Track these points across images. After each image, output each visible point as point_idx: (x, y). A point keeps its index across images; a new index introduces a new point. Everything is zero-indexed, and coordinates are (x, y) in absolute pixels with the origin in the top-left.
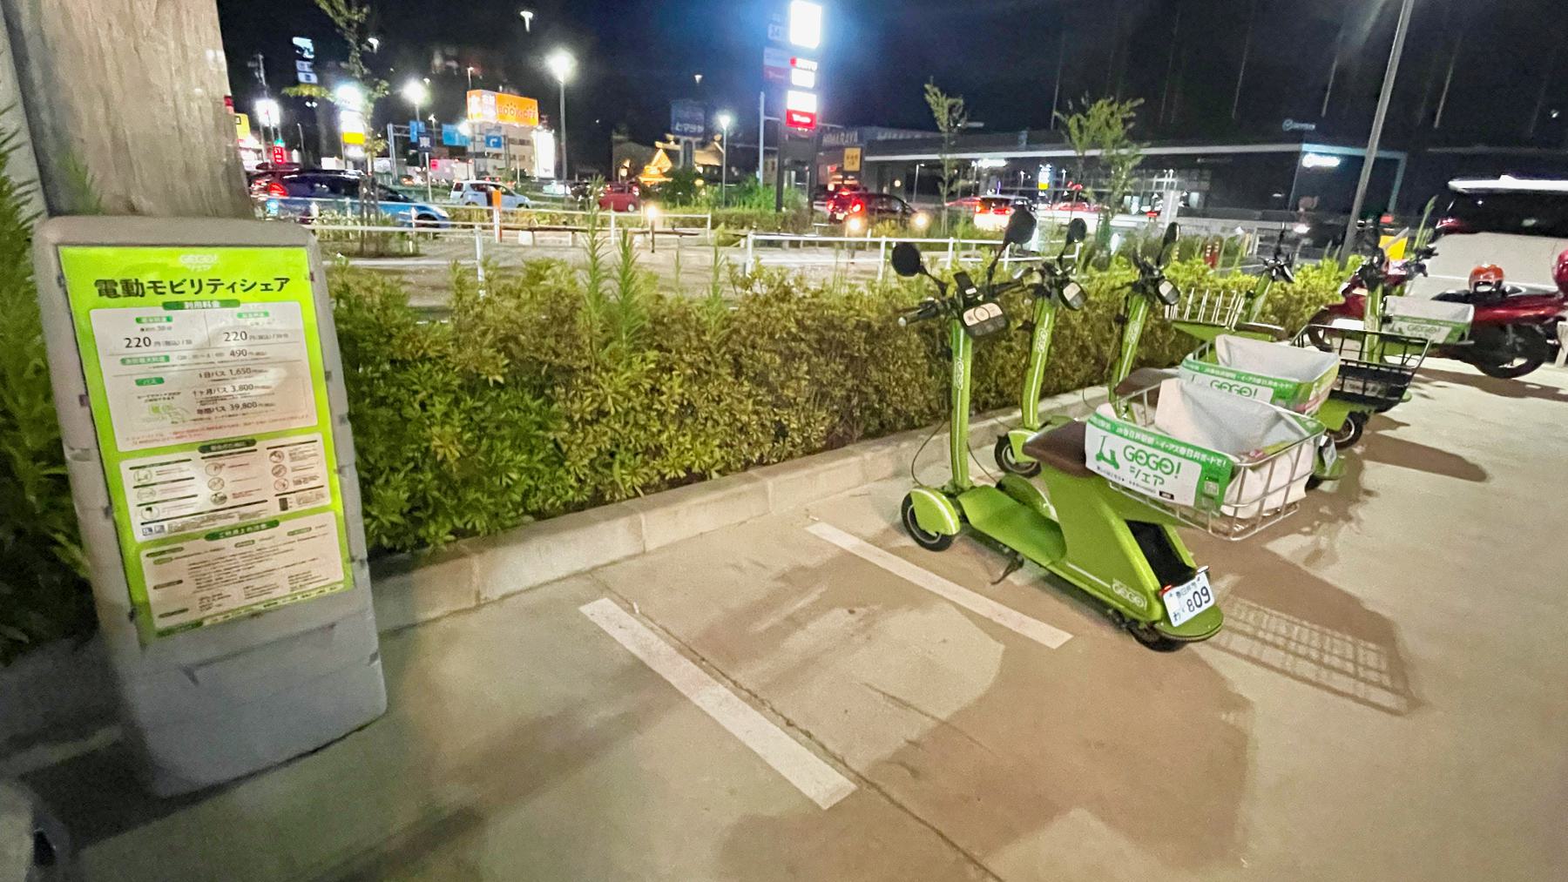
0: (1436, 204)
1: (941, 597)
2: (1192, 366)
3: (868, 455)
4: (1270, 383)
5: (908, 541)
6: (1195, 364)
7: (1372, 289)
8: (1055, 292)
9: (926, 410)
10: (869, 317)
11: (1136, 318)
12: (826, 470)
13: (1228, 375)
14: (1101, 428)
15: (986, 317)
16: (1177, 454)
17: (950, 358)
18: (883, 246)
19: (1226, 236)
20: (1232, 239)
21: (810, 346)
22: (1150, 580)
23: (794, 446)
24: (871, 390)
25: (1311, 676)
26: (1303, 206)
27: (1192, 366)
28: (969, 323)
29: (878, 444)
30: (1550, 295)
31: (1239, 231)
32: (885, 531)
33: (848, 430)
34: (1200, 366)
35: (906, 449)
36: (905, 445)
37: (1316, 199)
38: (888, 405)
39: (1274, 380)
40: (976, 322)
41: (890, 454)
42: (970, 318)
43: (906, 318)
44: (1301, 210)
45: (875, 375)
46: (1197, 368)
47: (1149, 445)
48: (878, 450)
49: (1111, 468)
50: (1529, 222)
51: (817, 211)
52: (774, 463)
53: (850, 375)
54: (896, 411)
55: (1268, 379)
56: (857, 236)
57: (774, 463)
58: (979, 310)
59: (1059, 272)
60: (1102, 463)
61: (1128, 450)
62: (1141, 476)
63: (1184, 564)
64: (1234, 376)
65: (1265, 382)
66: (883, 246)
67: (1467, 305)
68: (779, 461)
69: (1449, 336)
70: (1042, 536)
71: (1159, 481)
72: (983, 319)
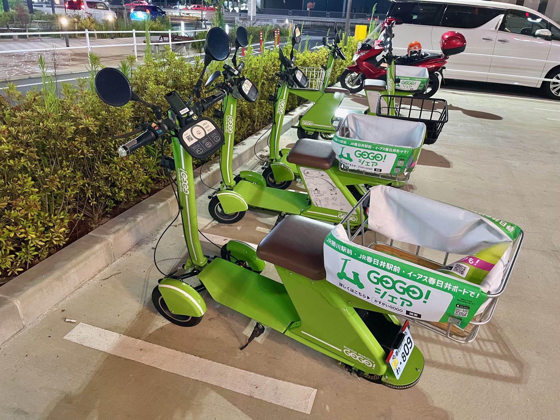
0: (376, 8)
1: (206, 384)
2: (342, 142)
3: (111, 238)
4: (394, 150)
5: (161, 322)
6: (344, 140)
7: (390, 64)
8: (235, 88)
9: (150, 180)
10: (86, 124)
11: (282, 98)
12: (74, 266)
13: (366, 146)
14: (341, 252)
15: (203, 135)
16: (427, 284)
17: (173, 168)
18: (87, 36)
19: (281, 25)
20: (283, 26)
21: (30, 159)
22: (377, 349)
23: (37, 249)
24: (102, 183)
25: (462, 364)
26: (309, 7)
27: (342, 142)
28: (189, 144)
29: (117, 224)
30: (440, 56)
31: (287, 21)
32: (140, 315)
33: (88, 214)
34: (347, 141)
35: (141, 221)
36: (140, 218)
37: (314, 3)
38: (120, 189)
39: (397, 148)
40: (195, 140)
41: (129, 230)
42: (189, 138)
43: (125, 148)
44: (308, 9)
45: (103, 170)
46: (345, 142)
47: (396, 273)
48: (119, 230)
49: (355, 287)
50: (415, 17)
51: (36, 10)
52: (20, 273)
53: (79, 174)
54: (127, 191)
55: (393, 148)
56: (68, 31)
57: (20, 273)
58: (196, 129)
59: (236, 72)
60: (344, 281)
61: (372, 275)
62: (387, 298)
63: (393, 323)
64: (370, 147)
65: (391, 150)
66: (87, 36)
67: (424, 68)
68: (25, 270)
69: (420, 86)
70: (271, 299)
71: (406, 303)
72: (200, 137)
